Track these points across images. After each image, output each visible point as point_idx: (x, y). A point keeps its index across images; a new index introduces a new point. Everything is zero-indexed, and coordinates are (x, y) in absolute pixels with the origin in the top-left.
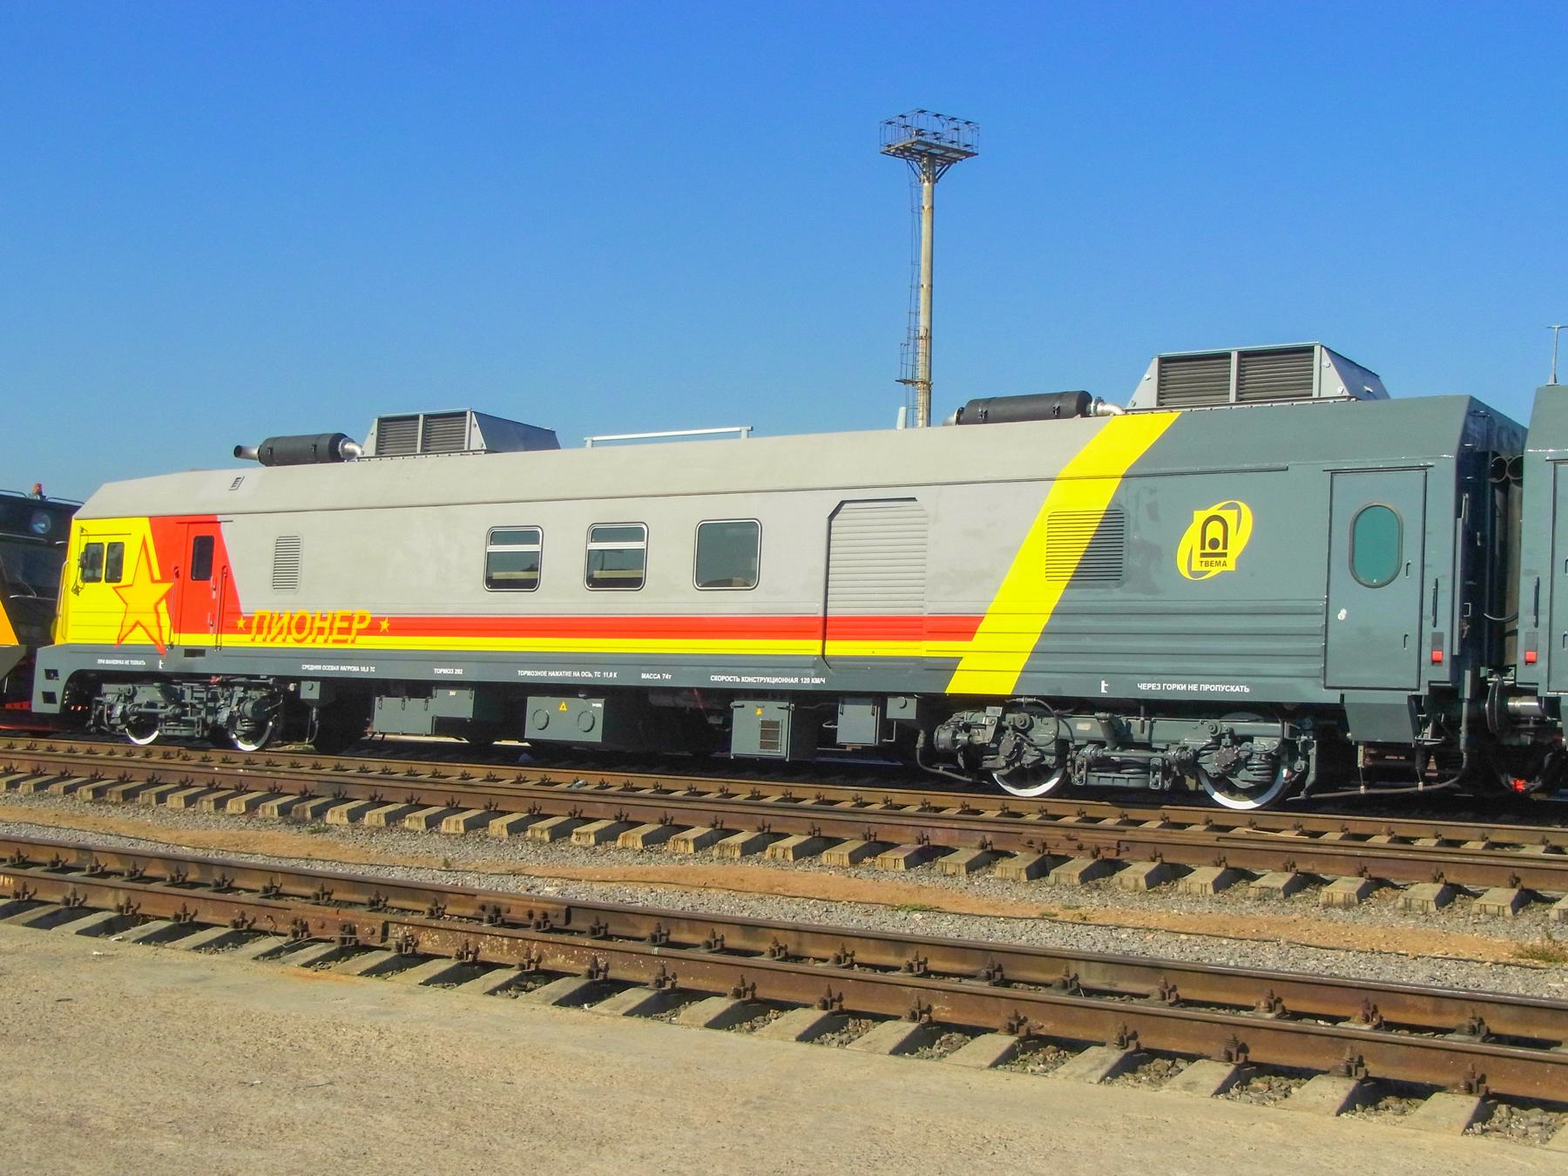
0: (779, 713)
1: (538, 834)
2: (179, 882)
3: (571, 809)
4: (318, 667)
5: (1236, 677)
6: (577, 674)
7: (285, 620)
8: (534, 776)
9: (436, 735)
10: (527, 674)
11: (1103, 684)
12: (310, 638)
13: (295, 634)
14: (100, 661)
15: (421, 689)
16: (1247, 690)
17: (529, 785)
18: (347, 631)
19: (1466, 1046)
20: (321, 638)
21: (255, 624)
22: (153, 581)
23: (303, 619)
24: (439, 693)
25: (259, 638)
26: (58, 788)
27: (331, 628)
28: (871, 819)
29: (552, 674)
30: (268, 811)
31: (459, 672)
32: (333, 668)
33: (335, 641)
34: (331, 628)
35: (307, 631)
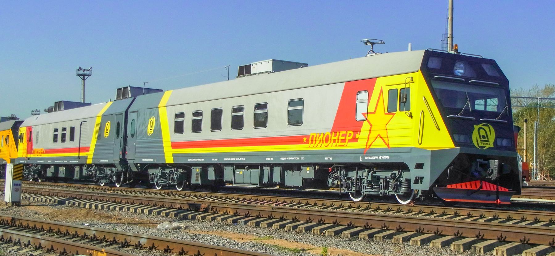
4: (285, 158)
5: (151, 157)
7: (321, 138)
10: (190, 160)
12: (331, 145)
13: (325, 144)
14: (143, 160)
15: (298, 167)
20: (334, 144)
22: (386, 114)
23: (328, 136)
24: (304, 168)
25: (312, 145)
26: (365, 234)
27: (338, 139)
30: (316, 231)
32: (290, 159)
34: (338, 139)
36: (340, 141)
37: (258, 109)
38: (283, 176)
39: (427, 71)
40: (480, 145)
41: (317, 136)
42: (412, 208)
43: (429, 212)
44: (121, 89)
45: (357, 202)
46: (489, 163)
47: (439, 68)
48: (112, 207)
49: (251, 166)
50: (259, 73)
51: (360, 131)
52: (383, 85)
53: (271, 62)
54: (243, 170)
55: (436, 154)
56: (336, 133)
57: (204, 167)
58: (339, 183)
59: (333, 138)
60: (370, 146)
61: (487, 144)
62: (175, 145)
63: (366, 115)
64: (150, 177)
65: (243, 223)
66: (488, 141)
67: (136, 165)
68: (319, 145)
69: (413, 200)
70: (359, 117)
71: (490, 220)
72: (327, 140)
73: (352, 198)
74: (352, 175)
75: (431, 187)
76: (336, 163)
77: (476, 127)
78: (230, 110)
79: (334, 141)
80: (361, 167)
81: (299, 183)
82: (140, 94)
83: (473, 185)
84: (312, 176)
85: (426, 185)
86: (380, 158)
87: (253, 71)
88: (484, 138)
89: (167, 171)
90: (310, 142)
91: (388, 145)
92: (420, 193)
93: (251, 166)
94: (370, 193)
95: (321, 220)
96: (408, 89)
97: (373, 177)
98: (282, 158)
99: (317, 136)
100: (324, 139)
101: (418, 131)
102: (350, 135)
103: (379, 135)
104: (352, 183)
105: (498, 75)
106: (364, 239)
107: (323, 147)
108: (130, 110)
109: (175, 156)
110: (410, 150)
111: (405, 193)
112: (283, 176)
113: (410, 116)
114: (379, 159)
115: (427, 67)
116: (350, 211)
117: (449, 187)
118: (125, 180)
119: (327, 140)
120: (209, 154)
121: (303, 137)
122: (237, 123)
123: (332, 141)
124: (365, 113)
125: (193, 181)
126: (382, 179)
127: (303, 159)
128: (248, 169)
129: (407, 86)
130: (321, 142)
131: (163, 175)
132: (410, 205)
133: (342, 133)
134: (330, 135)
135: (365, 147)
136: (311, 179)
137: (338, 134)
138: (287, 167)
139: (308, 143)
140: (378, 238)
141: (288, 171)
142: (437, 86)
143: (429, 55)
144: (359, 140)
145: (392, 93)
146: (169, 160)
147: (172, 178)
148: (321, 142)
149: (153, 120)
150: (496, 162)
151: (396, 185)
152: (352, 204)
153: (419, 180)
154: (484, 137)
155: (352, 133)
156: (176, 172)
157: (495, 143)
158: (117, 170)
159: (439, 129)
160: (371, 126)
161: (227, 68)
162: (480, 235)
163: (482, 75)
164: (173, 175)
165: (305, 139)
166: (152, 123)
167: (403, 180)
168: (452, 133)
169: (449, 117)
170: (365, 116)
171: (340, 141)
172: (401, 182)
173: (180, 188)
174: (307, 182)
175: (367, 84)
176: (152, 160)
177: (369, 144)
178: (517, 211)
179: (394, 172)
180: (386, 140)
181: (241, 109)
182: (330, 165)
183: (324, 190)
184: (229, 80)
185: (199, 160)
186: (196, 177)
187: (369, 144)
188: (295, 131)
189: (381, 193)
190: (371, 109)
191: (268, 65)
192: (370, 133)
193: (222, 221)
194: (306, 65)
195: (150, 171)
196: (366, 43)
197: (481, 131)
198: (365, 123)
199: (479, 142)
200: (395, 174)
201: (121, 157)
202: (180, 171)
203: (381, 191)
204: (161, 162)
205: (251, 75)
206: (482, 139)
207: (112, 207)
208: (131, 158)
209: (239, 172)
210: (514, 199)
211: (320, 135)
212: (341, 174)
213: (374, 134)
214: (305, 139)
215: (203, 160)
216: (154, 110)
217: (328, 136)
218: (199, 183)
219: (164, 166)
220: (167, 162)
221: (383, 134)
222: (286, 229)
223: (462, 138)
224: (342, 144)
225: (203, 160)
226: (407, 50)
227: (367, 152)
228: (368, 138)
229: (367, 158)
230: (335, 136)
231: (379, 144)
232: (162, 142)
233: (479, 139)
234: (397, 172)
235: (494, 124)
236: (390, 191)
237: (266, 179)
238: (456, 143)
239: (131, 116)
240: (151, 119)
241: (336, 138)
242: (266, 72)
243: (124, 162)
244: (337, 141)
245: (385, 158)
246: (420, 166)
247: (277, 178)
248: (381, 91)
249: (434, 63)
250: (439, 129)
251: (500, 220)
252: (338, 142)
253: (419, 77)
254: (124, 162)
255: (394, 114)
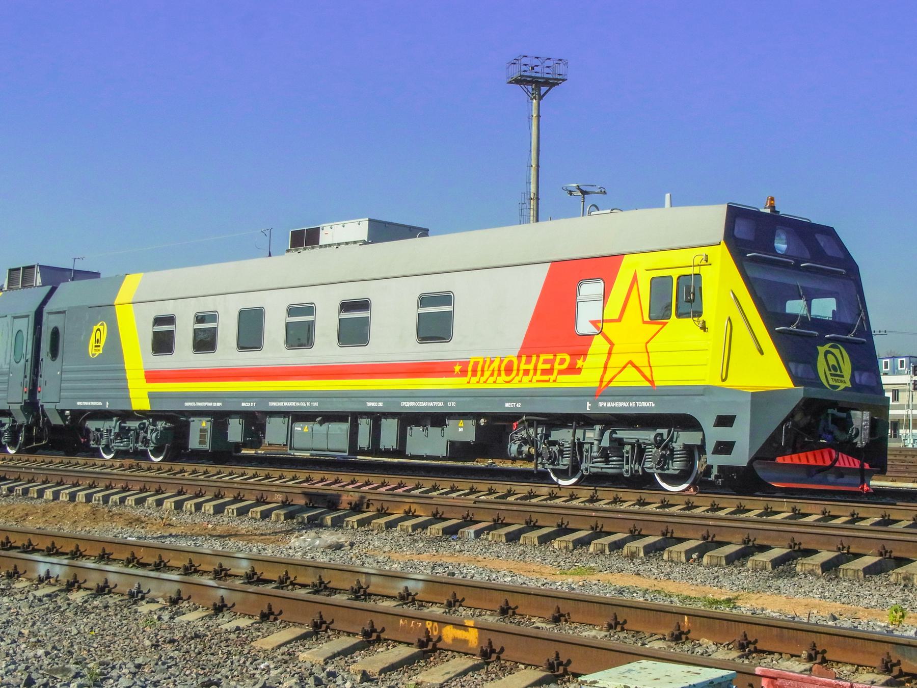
0: (205, 423)
1: (674, 556)
2: (132, 561)
3: (704, 533)
4: (412, 404)
5: (97, 399)
6: (298, 404)
7: (496, 364)
8: (262, 472)
9: (450, 459)
10: (189, 405)
11: (588, 405)
12: (518, 378)
13: (504, 377)
14: (79, 403)
15: (438, 419)
16: (653, 405)
17: (624, 507)
18: (549, 372)
19: (399, 610)
21: (470, 368)
22: (645, 322)
23: (510, 363)
24: (451, 423)
25: (474, 380)
27: (535, 369)
28: (200, 483)
29: (286, 404)
31: (381, 404)
32: (423, 404)
33: (538, 381)
34: (535, 369)
35: (515, 372)
36: (539, 372)
37: (345, 311)
38: (402, 438)
39: (733, 241)
40: (831, 383)
41: (485, 362)
42: (692, 499)
43: (349, 481)
44: (19, 269)
45: (566, 487)
46: (849, 416)
47: (752, 236)
48: (116, 498)
49: (329, 417)
50: (339, 244)
51: (585, 355)
52: (640, 270)
53: (365, 224)
54: (311, 424)
55: (761, 400)
56: (529, 357)
57: (220, 419)
58: (533, 451)
59: (523, 366)
60: (610, 381)
61: (841, 381)
62: (152, 376)
63: (600, 325)
64: (91, 435)
65: (473, 536)
66: (842, 376)
67: (61, 412)
68: (492, 379)
69: (693, 484)
70: (583, 327)
71: (504, 497)
72: (509, 370)
73: (555, 479)
74: (564, 436)
75: (751, 462)
76: (527, 414)
77: (821, 350)
78: (192, 319)
79: (526, 372)
80: (585, 421)
81: (442, 451)
82: (66, 281)
83: (819, 457)
84: (471, 437)
85: (740, 457)
86: (632, 404)
87: (323, 239)
88: (835, 369)
89: (134, 425)
90: (470, 374)
91: (652, 382)
92: (715, 472)
93: (329, 417)
94: (604, 470)
95: (410, 510)
96: (698, 276)
97: (612, 440)
98: (403, 404)
99: (485, 362)
100: (503, 368)
101: (724, 356)
102: (562, 361)
103: (631, 362)
104: (561, 452)
105: (841, 255)
106: (812, 572)
107: (501, 383)
108: (47, 309)
109: (152, 396)
110: (706, 390)
111: (681, 470)
112: (402, 438)
113: (704, 328)
114: (630, 407)
115: (734, 236)
116: (11, 464)
117: (779, 460)
118: (28, 440)
119: (509, 370)
120: (412, 391)
121: (454, 364)
122: (205, 342)
123: (521, 372)
124: (598, 321)
125: (194, 443)
126: (629, 444)
127: (452, 405)
128: (321, 423)
129: (696, 270)
130: (496, 373)
131: (123, 433)
132: (687, 493)
133: (543, 357)
134: (515, 361)
135: (597, 385)
136: (468, 443)
137: (534, 358)
138: (409, 420)
139: (466, 376)
140: (850, 573)
141: (414, 428)
142: (755, 272)
143: (735, 214)
144: (583, 371)
145: (659, 285)
146: (140, 401)
147: (145, 437)
148: (496, 373)
149: (101, 328)
150: (866, 415)
151: (663, 456)
152: (556, 491)
153: (725, 447)
154: (834, 368)
155: (568, 358)
156: (151, 427)
157: (852, 379)
158: (14, 421)
159: (762, 353)
160: (612, 344)
161: (267, 233)
162: (750, 540)
163: (818, 254)
164: (146, 432)
165: (457, 368)
166: (100, 332)
167: (677, 446)
168: (786, 360)
169: (779, 332)
170: (597, 328)
171: (539, 372)
172: (672, 450)
173: (157, 457)
174: (457, 449)
175: (604, 267)
176: (100, 404)
177: (607, 378)
178: (895, 505)
179: (659, 431)
180: (647, 372)
181: (170, 320)
182: (514, 417)
183: (396, 460)
184: (270, 255)
185: (210, 404)
186: (199, 434)
187: (607, 378)
188: (434, 352)
189: (627, 471)
190: (613, 311)
191: (359, 229)
192: (608, 358)
193: (414, 530)
194: (425, 233)
195: (92, 425)
196: (571, 193)
197: (830, 356)
198: (598, 341)
199: (829, 376)
200: (662, 435)
201: (26, 397)
202: (161, 425)
203: (626, 467)
204: (120, 406)
205: (321, 247)
206: (833, 372)
207: (116, 498)
208: (48, 399)
209: (301, 428)
210: (875, 483)
211: (492, 362)
212: (537, 434)
213: (617, 361)
214: (457, 368)
215: (219, 404)
216: (105, 311)
217: (510, 363)
218: (207, 447)
219: (128, 415)
220: (134, 408)
221: (640, 360)
222: (591, 549)
223: (800, 369)
224: (546, 378)
225: (219, 404)
226: (662, 205)
227: (602, 392)
228: (605, 368)
229: (601, 404)
230: (528, 362)
231: (630, 379)
232: (124, 370)
233: (828, 373)
234: (665, 431)
235: (846, 343)
236: (140, 446)
237: (364, 441)
238: (796, 380)
239: (49, 323)
240: (98, 326)
241: (531, 367)
242: (355, 242)
243: (32, 406)
244: (531, 372)
245: (647, 406)
246: (725, 421)
247: (388, 439)
248: (635, 279)
249: (743, 230)
250: (762, 353)
251: (442, 491)
252: (535, 374)
253: (721, 256)
254: (32, 406)
255: (665, 324)
